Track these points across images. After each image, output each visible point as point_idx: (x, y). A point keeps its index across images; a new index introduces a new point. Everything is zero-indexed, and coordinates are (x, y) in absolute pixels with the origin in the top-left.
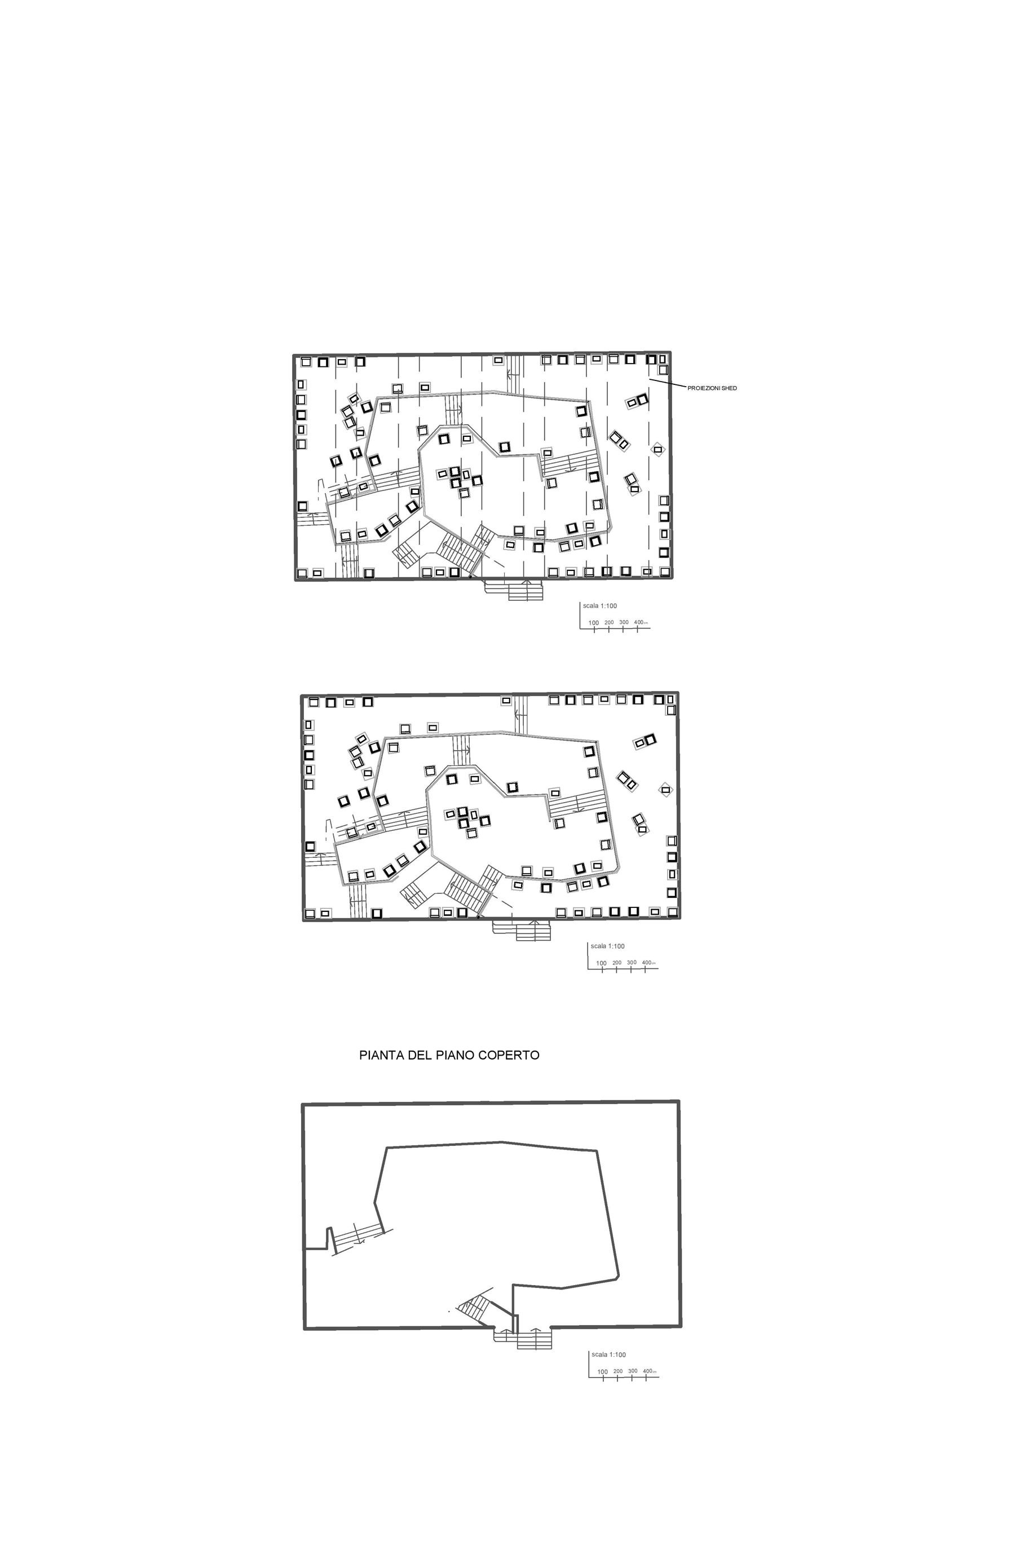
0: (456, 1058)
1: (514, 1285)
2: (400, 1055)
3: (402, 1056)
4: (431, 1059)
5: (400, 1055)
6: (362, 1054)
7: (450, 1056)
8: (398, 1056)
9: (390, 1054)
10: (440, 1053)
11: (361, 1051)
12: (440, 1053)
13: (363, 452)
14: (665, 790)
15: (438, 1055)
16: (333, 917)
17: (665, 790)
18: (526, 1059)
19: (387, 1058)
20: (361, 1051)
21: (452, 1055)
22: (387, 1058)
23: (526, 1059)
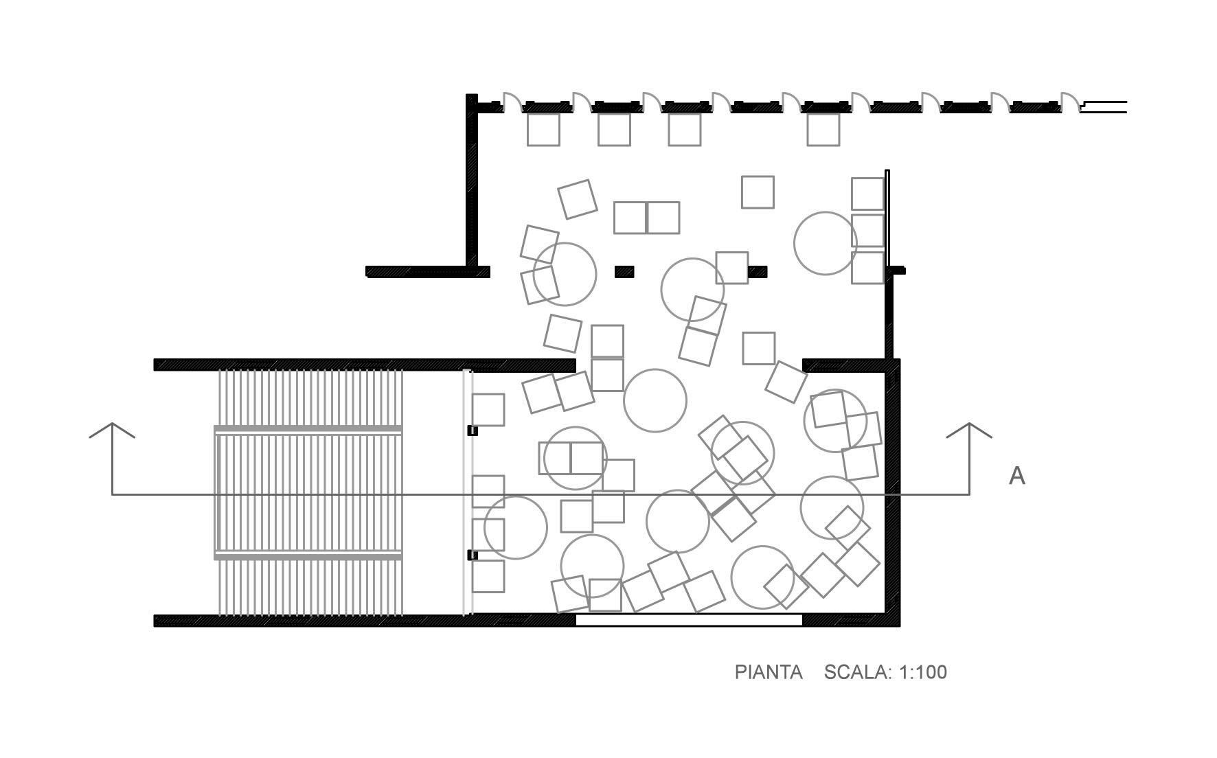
0: (766, 676)
1: (679, 202)
2: (881, 671)
3: (799, 673)
4: (737, 678)
5: (796, 671)
6: (740, 670)
7: (756, 673)
8: (794, 673)
9: (781, 670)
10: (741, 669)
11: (737, 666)
12: (741, 669)
13: (681, 369)
14: (901, 270)
15: (737, 672)
16: (216, 373)
17: (901, 270)
18: (921, 678)
19: (776, 677)
20: (737, 666)
21: (759, 671)
22: (776, 677)
23: (921, 678)
